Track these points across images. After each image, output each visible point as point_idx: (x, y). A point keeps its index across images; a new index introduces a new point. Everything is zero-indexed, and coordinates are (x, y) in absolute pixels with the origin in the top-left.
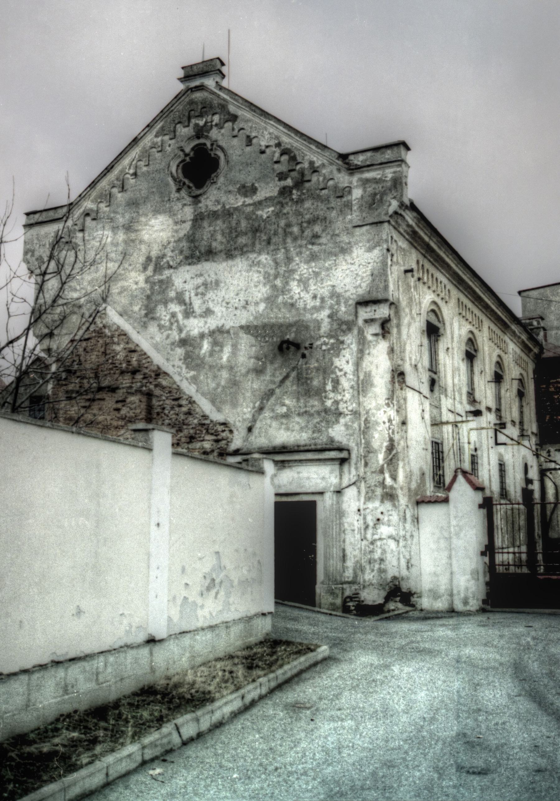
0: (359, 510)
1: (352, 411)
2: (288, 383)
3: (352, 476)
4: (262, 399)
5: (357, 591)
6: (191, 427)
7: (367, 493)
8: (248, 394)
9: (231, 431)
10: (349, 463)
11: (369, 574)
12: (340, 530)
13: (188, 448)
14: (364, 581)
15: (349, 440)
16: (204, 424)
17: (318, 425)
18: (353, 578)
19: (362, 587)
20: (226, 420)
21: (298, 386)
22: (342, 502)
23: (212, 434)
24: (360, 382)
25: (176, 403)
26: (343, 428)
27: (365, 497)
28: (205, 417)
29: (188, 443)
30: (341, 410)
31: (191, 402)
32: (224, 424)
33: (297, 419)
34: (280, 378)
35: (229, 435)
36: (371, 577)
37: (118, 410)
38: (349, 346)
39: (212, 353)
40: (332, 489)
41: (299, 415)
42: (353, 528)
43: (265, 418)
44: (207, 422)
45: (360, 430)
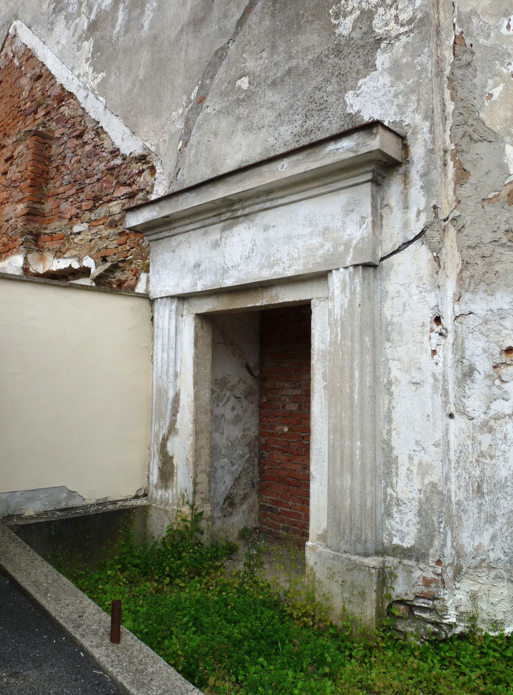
0: (438, 320)
1: (410, 21)
2: (253, 18)
3: (412, 214)
4: (203, 79)
5: (433, 588)
6: (96, 177)
7: (466, 264)
8: (180, 80)
9: (153, 169)
10: (406, 175)
11: (478, 530)
12: (375, 379)
13: (89, 221)
14: (459, 554)
15: (401, 109)
16: (113, 168)
17: (318, 95)
18: (419, 539)
19: (450, 573)
20: (145, 148)
21: (273, 15)
22: (385, 294)
23: (125, 184)
24: (453, 456)
25: (79, 142)
26: (386, 79)
27: (460, 279)
28: (115, 152)
29: (90, 210)
30: (379, 31)
31: (99, 131)
32: (142, 158)
33: (271, 96)
34: (238, 15)
35: (149, 178)
36: (485, 539)
37: (5, 173)
38: (438, 575)
39: (127, 27)
40: (349, 261)
41: (274, 84)
42: (417, 377)
43: (206, 120)
44: (118, 161)
45: (439, 73)
